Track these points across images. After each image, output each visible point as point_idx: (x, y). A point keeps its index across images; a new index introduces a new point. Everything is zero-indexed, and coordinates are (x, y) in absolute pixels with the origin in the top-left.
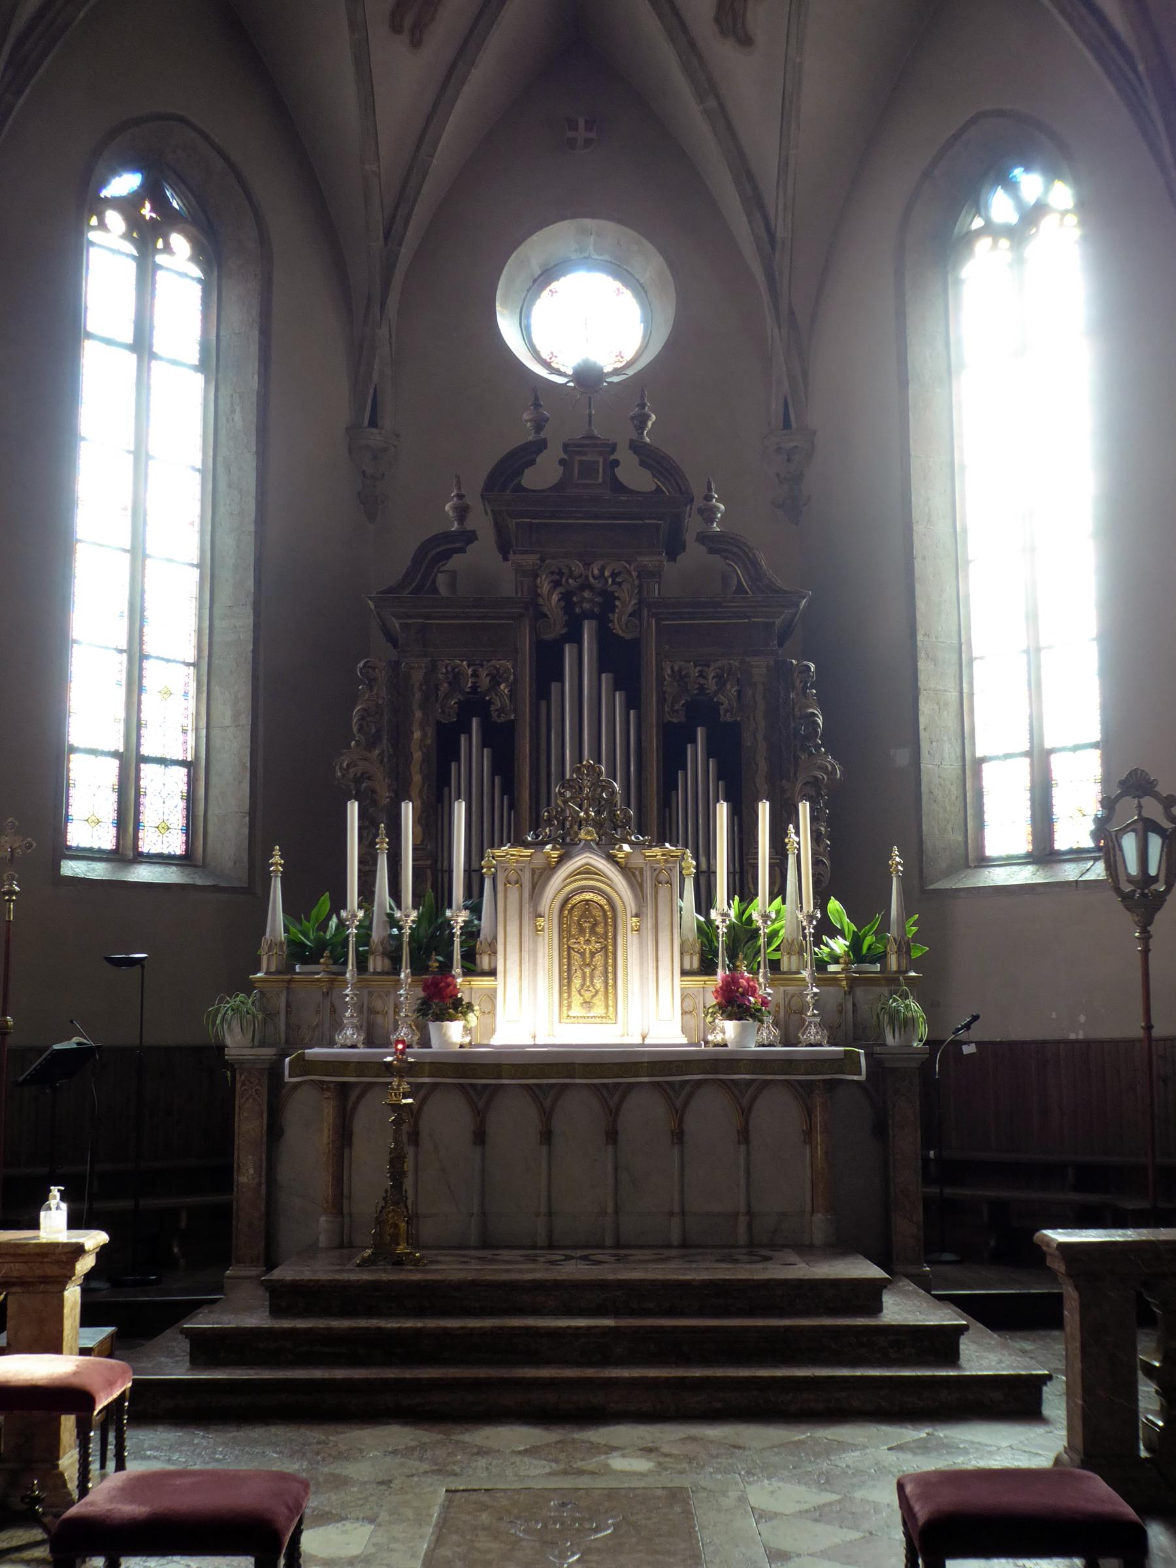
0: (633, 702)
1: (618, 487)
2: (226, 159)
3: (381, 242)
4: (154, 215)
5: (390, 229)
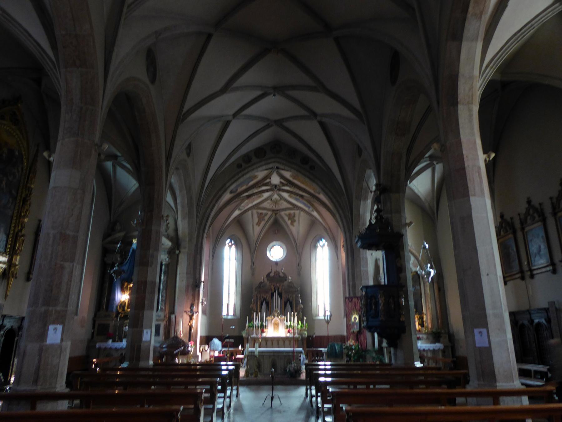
0: (281, 299)
1: (280, 276)
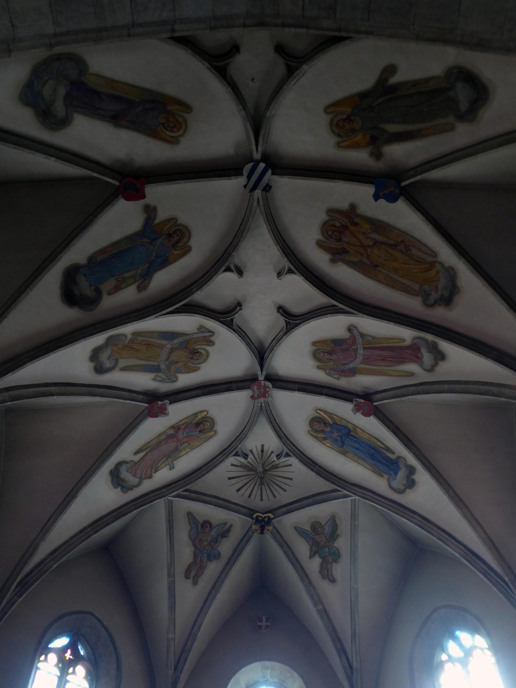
2: (107, 630)
3: (173, 671)
4: (71, 657)
5: (177, 665)
